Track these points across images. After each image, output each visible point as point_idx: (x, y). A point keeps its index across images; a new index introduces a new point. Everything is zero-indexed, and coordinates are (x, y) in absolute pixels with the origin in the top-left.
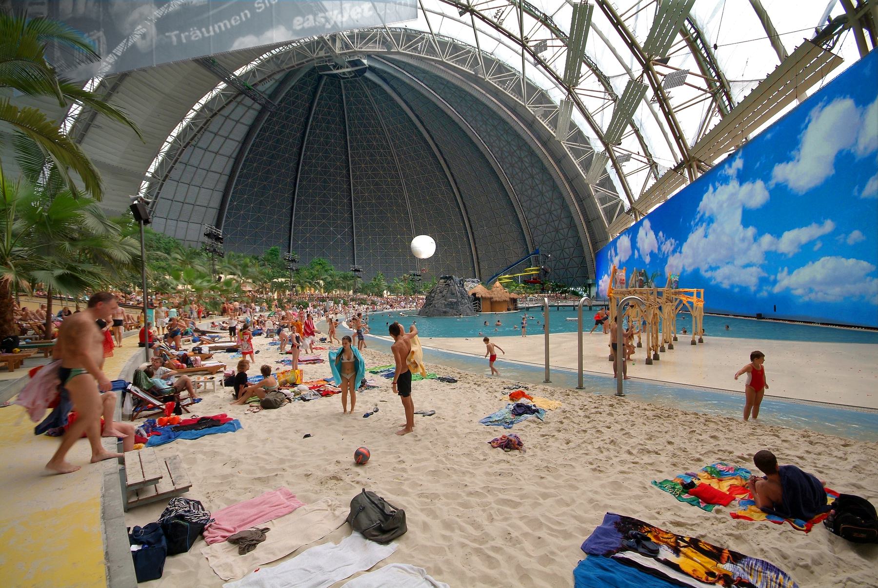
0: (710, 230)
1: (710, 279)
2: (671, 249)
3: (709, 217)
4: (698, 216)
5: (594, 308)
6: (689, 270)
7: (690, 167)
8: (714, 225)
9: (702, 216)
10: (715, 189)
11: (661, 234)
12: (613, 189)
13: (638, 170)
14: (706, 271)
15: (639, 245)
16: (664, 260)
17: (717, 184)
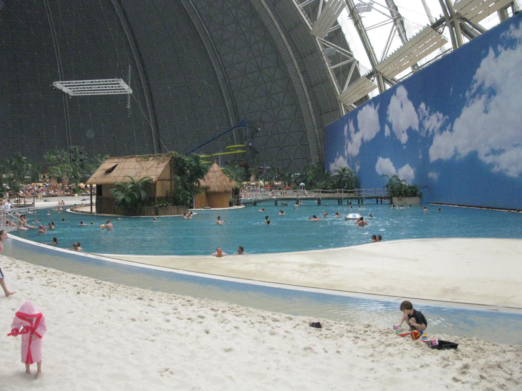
0: (492, 105)
1: (492, 165)
2: (439, 125)
3: (490, 88)
4: (475, 86)
5: (279, 203)
6: (464, 152)
7: (452, 25)
8: (497, 98)
9: (480, 87)
10: (497, 54)
11: (423, 106)
12: (346, 46)
13: (383, 24)
14: (487, 155)
15: (391, 118)
16: (428, 140)
17: (500, 48)
